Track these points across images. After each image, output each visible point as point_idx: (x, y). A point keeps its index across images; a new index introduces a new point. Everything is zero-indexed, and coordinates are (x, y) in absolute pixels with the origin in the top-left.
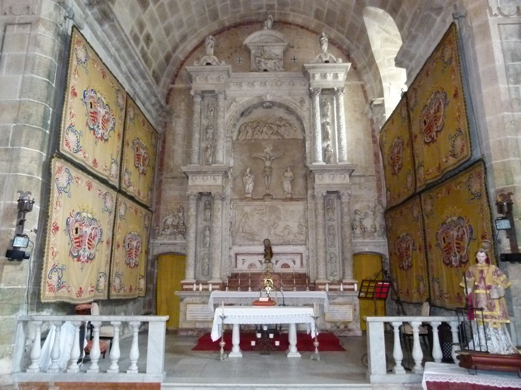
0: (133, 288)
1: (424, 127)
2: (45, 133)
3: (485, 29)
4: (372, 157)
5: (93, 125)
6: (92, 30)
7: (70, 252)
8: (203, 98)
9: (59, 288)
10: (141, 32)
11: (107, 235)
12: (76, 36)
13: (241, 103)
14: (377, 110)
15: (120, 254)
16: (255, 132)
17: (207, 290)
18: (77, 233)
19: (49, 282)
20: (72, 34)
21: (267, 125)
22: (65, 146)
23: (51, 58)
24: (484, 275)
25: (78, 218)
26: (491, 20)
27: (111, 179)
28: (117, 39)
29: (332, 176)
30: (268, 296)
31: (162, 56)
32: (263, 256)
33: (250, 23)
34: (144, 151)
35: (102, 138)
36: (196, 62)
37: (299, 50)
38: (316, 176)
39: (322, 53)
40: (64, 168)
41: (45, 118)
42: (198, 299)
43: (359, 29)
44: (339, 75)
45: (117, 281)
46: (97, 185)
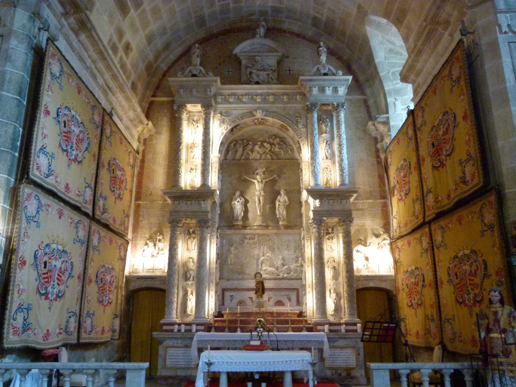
1: (432, 150)
2: (14, 155)
3: (495, 47)
4: (377, 180)
5: (67, 146)
6: (67, 41)
7: (38, 289)
10: (120, 40)
11: (78, 269)
12: (51, 50)
17: (190, 331)
18: (45, 267)
19: (14, 324)
20: (46, 48)
22: (35, 170)
23: (23, 74)
24: (499, 317)
25: (47, 250)
26: (501, 38)
28: (94, 50)
30: (260, 339)
32: (254, 292)
33: (240, 30)
35: (75, 160)
36: (181, 73)
39: (320, 64)
40: (33, 195)
41: (14, 140)
42: (179, 341)
44: (339, 89)
46: (69, 213)
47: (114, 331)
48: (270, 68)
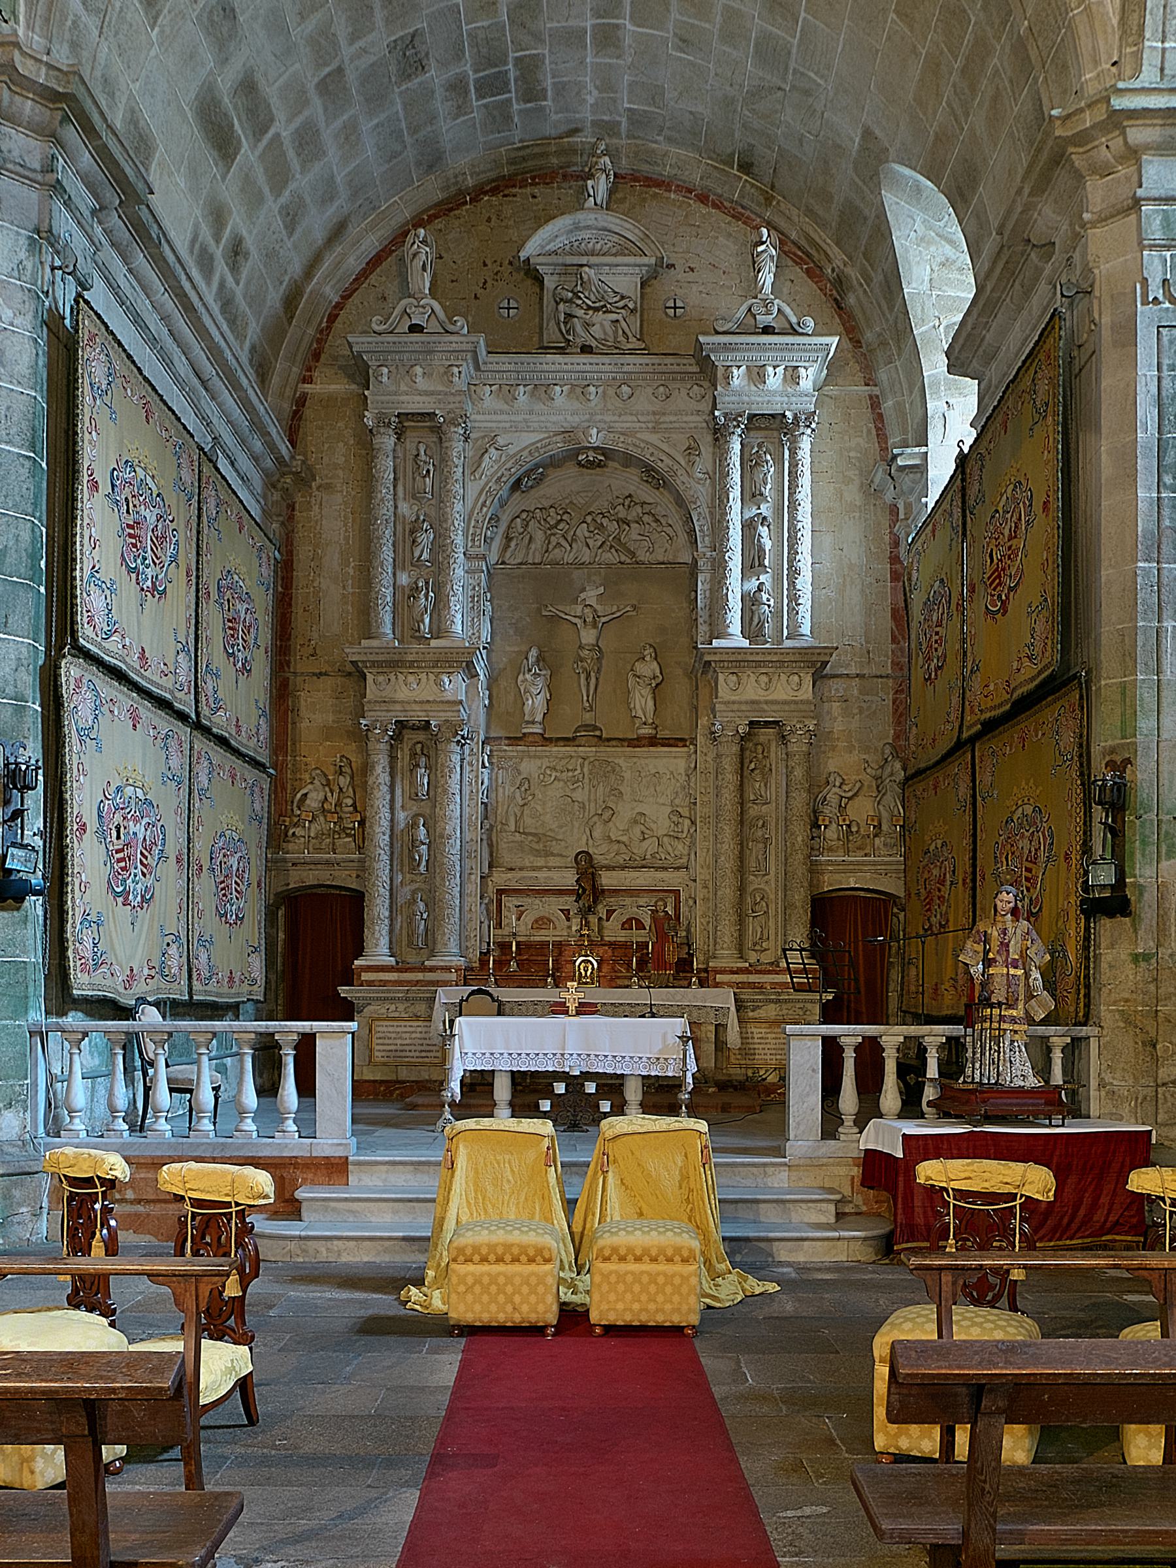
0: (237, 976)
8: (400, 435)
9: (97, 966)
11: (175, 843)
12: (87, 325)
13: (512, 450)
14: (907, 480)
15: (205, 886)
16: (554, 540)
21: (589, 519)
27: (179, 695)
29: (764, 679)
31: (274, 297)
34: (246, 606)
37: (691, 276)
38: (721, 677)
41: (34, 558)
42: (401, 1007)
43: (870, 222)
45: (203, 957)
47: (254, 982)
48: (621, 304)
